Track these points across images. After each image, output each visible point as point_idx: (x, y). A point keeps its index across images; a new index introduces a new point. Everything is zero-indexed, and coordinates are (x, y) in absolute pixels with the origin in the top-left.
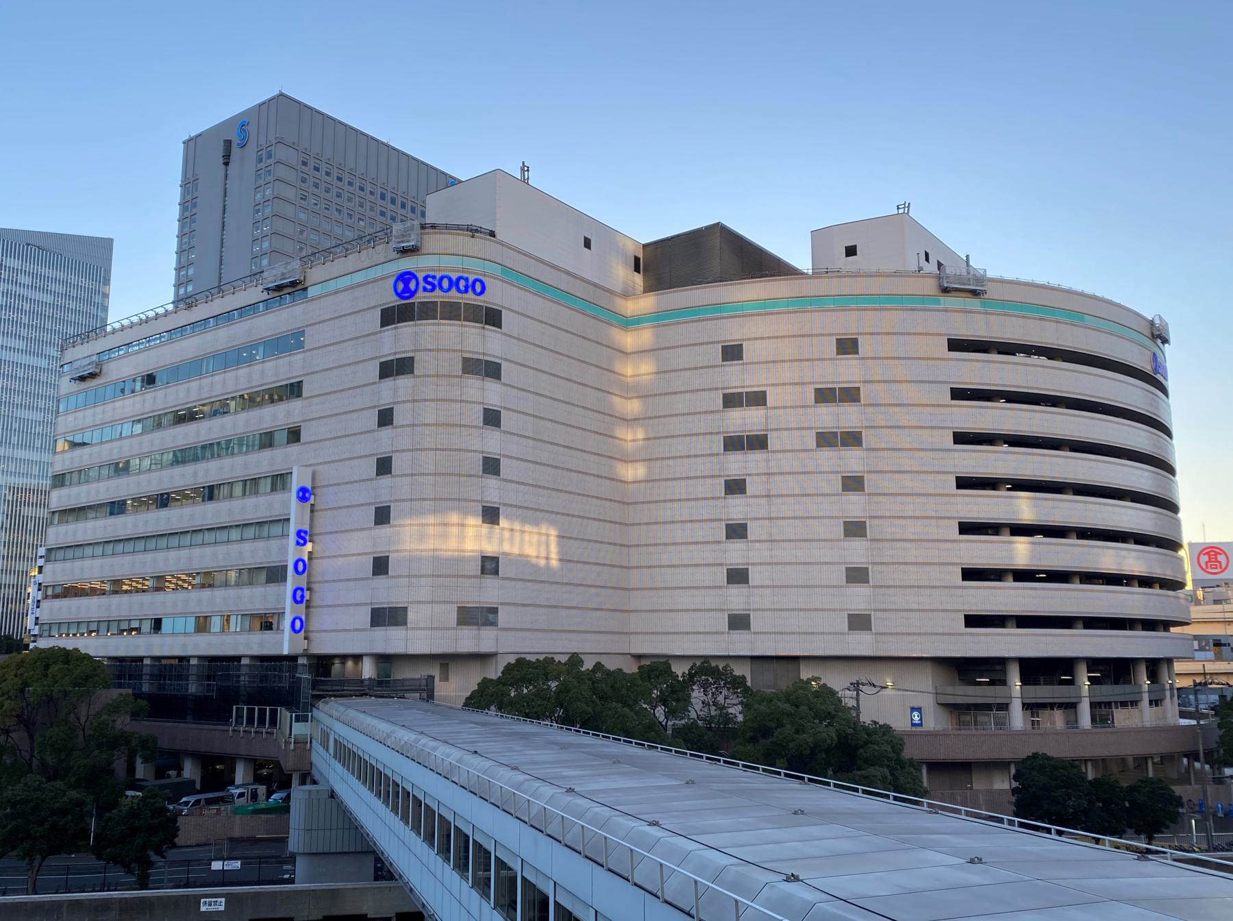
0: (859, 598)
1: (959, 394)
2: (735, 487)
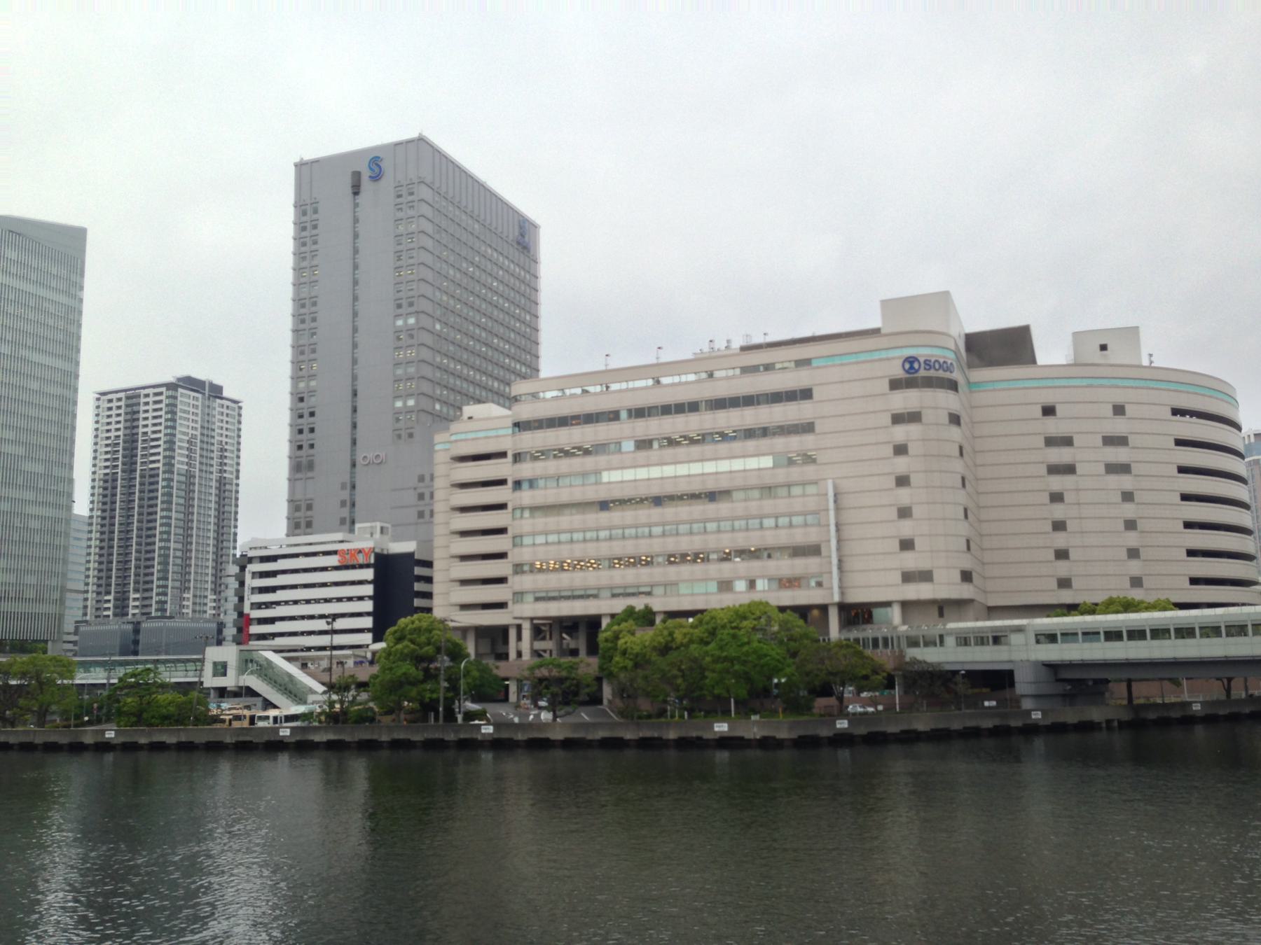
0: (1135, 568)
1: (1180, 443)
2: (1057, 498)
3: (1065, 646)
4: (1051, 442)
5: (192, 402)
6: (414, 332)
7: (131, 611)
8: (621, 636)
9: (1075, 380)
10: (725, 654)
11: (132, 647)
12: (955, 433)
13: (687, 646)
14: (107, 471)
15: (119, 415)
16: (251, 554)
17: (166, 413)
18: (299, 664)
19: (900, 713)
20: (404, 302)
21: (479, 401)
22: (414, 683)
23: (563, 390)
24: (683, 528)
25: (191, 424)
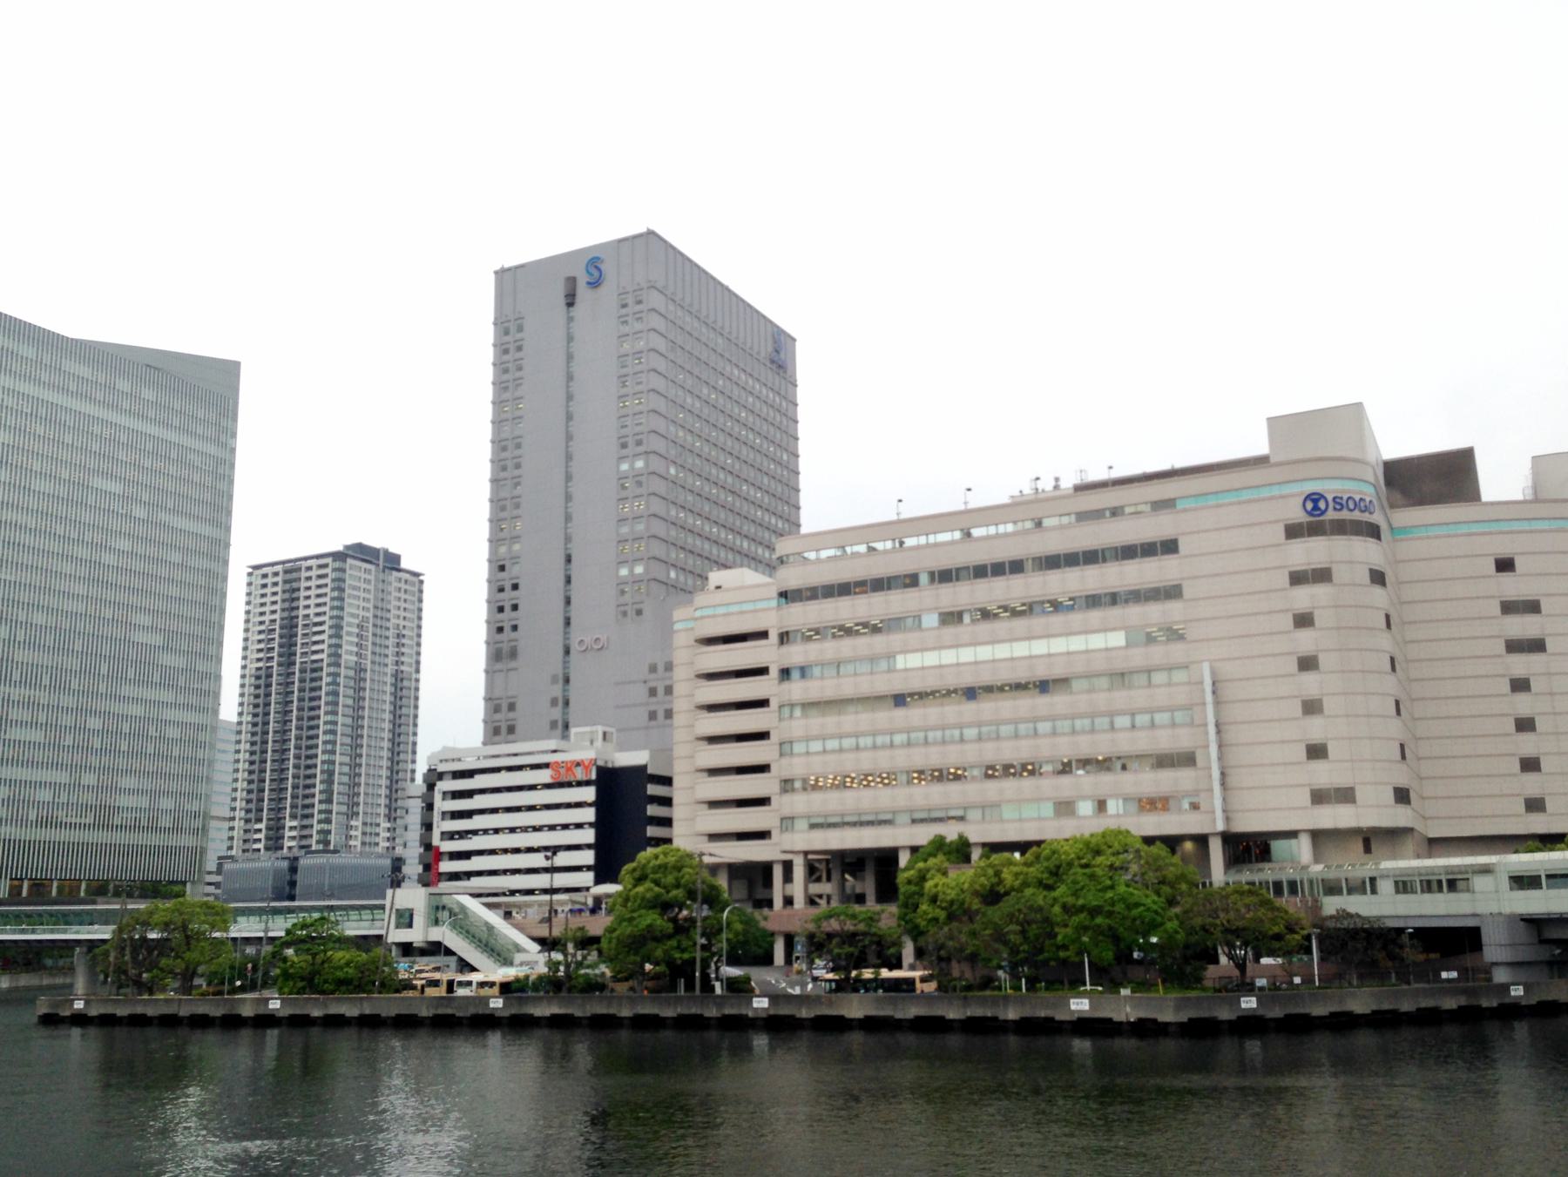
2: (1520, 685)
3: (1553, 892)
4: (1508, 608)
5: (363, 576)
6: (643, 479)
7: (287, 843)
8: (928, 876)
9: (1540, 522)
10: (1081, 902)
11: (287, 888)
13: (1020, 890)
14: (260, 664)
15: (275, 594)
16: (441, 768)
17: (333, 590)
18: (501, 912)
19: (1319, 988)
21: (726, 567)
22: (660, 939)
23: (843, 547)
24: (1006, 730)
25: (362, 604)
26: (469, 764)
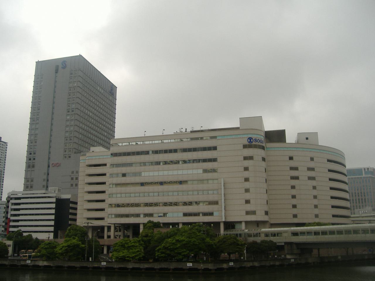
2: (293, 187)
4: (292, 169)
12: (263, 164)
20: (70, 111)
21: (94, 146)
26: (20, 195)
